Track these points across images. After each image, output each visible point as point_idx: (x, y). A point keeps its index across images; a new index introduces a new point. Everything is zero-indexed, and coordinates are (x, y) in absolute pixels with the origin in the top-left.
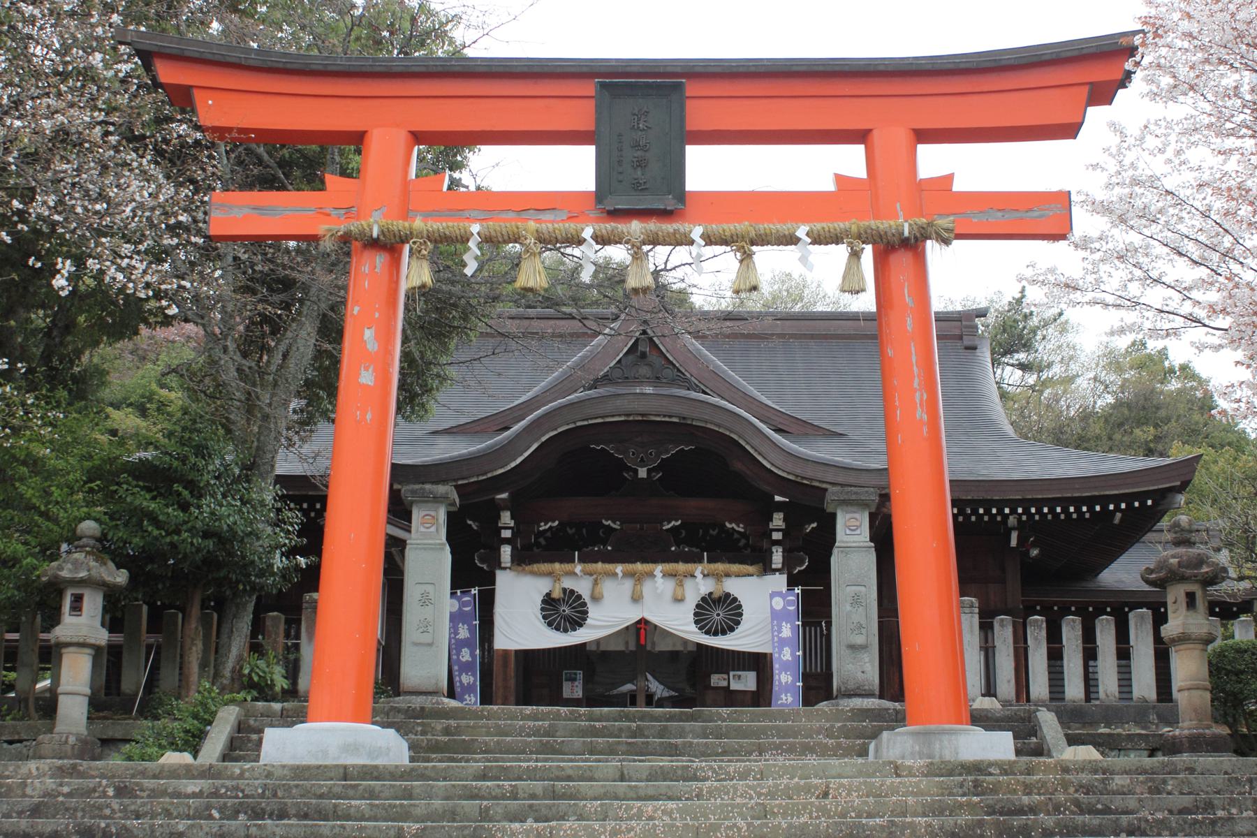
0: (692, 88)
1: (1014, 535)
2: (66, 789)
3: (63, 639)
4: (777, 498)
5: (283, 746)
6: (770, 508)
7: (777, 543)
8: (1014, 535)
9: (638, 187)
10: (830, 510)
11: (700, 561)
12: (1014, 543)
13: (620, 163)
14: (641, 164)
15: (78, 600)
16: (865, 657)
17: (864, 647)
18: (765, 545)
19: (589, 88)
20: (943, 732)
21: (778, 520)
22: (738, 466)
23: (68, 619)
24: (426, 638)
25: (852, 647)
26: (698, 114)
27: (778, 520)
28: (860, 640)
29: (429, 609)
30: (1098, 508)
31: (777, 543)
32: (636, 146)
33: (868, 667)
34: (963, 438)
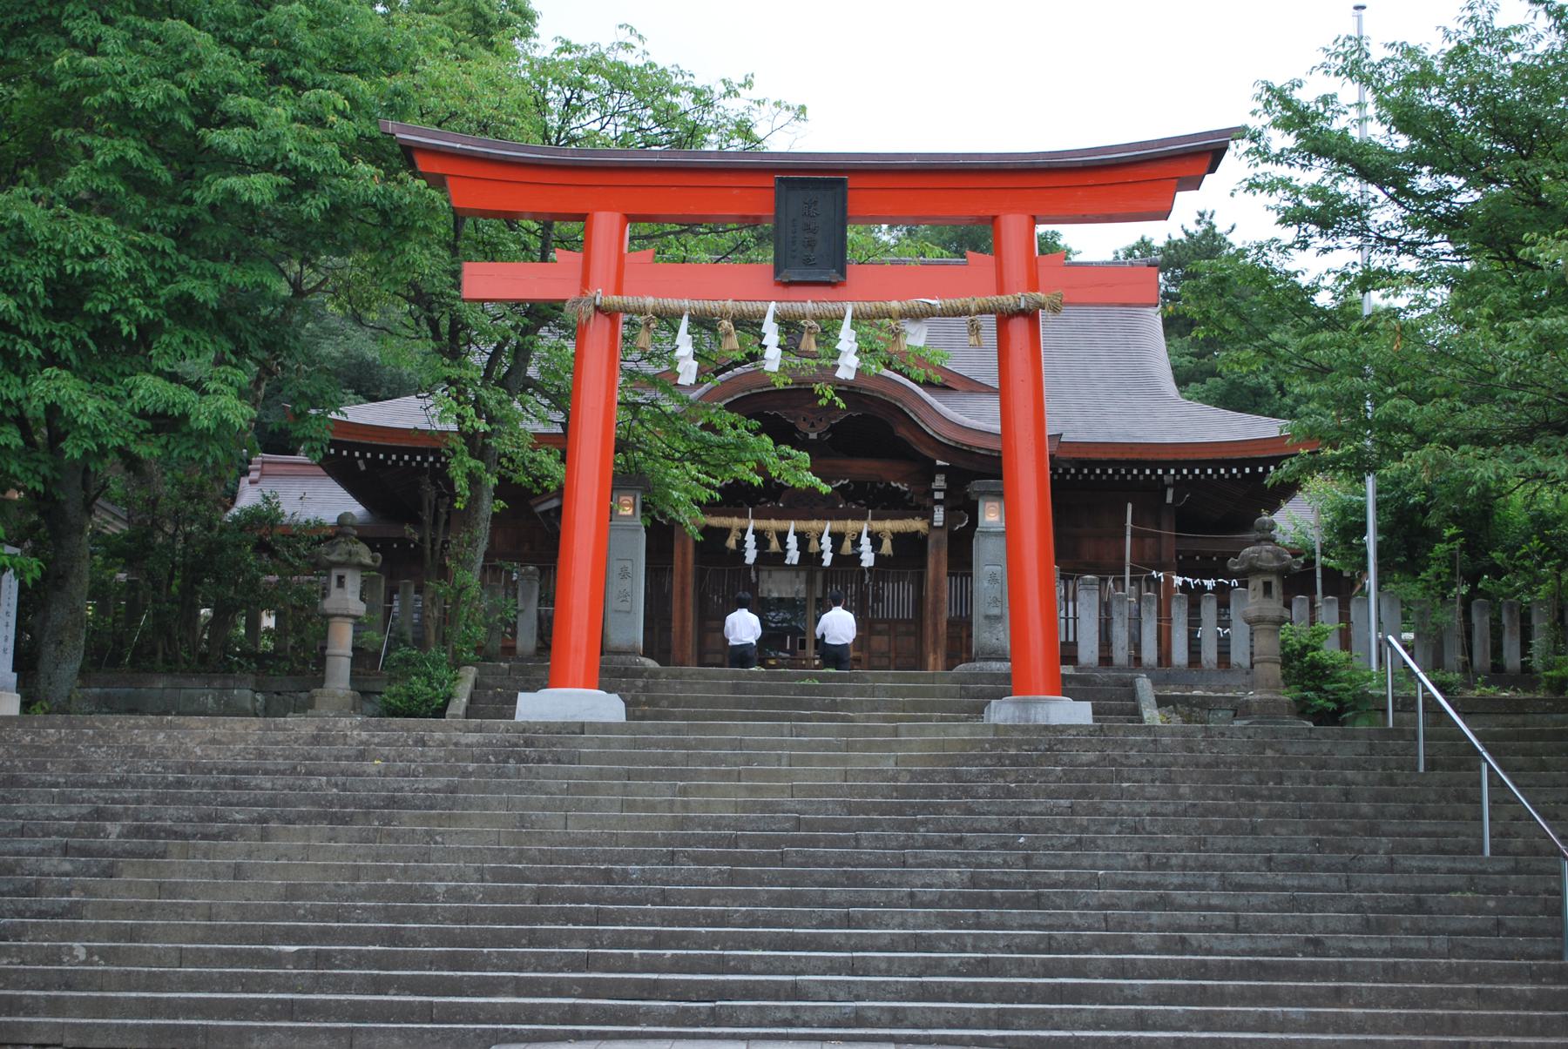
0: (851, 182)
1: (1170, 493)
2: (376, 740)
3: (331, 611)
4: (939, 462)
5: (534, 706)
6: (933, 470)
7: (939, 502)
8: (1170, 493)
9: (808, 262)
10: (973, 497)
11: (864, 518)
12: (1169, 499)
13: (794, 243)
14: (810, 244)
15: (341, 580)
16: (1000, 627)
17: (998, 618)
18: (928, 503)
19: (769, 181)
20: (1039, 701)
21: (940, 482)
22: (902, 432)
23: (335, 592)
24: (625, 606)
25: (987, 617)
26: (855, 202)
27: (940, 482)
28: (996, 611)
29: (627, 583)
30: (1247, 470)
31: (939, 502)
32: (807, 228)
33: (1002, 635)
34: (1124, 397)
